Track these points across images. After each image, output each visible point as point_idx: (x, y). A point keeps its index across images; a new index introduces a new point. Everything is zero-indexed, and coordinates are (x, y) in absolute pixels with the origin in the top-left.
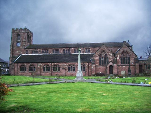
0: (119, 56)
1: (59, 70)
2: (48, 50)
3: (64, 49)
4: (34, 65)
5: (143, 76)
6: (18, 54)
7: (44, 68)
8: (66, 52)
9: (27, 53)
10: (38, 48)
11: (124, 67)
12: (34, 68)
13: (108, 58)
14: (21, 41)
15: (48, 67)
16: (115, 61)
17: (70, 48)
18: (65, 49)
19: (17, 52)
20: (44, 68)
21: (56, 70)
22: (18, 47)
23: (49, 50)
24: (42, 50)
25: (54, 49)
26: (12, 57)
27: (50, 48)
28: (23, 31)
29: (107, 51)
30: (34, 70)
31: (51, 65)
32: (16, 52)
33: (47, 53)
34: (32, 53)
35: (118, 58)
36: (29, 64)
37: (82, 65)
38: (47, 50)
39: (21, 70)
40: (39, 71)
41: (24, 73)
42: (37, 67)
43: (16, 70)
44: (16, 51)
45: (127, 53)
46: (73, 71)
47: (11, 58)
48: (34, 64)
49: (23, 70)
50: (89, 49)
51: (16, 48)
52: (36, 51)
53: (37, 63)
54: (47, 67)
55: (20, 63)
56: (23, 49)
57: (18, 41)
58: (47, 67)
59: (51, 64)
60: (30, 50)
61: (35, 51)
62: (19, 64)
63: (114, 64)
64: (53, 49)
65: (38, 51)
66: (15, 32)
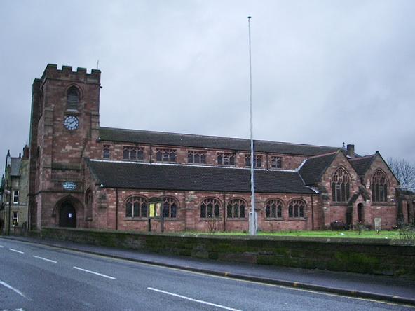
0: (369, 183)
1: (280, 215)
2: (175, 151)
3: (218, 153)
4: (172, 199)
5: (74, 242)
6: (70, 156)
7: (203, 207)
8: (165, 160)
9: (106, 156)
10: (144, 144)
11: (379, 208)
12: (142, 207)
14: (84, 114)
16: (362, 192)
17: (235, 151)
18: (222, 154)
19: (69, 148)
20: (202, 210)
21: (236, 215)
22: (71, 132)
23: (179, 150)
24: (157, 150)
25: (192, 152)
26: (52, 164)
27: (184, 147)
28: (89, 80)
29: (347, 167)
30: (173, 216)
31: (224, 199)
32: (63, 150)
33: (174, 160)
34: (126, 156)
36: (158, 192)
37: (168, 200)
38: (171, 150)
39: (128, 214)
40: (191, 216)
41: (140, 223)
42: (185, 205)
43: (114, 212)
44: (63, 145)
45: (381, 174)
46: (277, 219)
48: (172, 194)
49: (136, 215)
50: (205, 153)
51: (66, 136)
52: (137, 151)
53: (185, 190)
54: (210, 206)
55: (125, 188)
56: (94, 142)
57: (69, 110)
59: (224, 196)
61: (133, 152)
62: (124, 192)
63: (365, 201)
64: (189, 151)
65: (146, 152)
66: (60, 77)
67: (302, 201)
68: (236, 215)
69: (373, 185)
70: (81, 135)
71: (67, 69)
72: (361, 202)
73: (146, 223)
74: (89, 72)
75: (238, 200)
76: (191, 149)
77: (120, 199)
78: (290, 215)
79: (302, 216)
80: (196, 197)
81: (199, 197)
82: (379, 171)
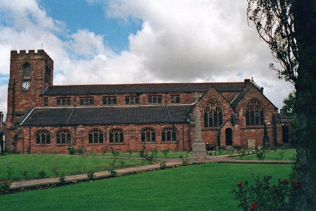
0: (242, 110)
1: (122, 140)
3: (126, 96)
7: (90, 136)
13: (221, 114)
15: (98, 133)
19: (24, 101)
21: (117, 141)
24: (80, 98)
35: (241, 113)
37: (149, 130)
44: (21, 100)
47: (11, 116)
56: (38, 97)
58: (96, 135)
60: (53, 99)
61: (155, 99)
63: (234, 126)
65: (72, 99)
67: (174, 129)
68: (117, 141)
69: (206, 115)
70: (31, 93)
71: (23, 52)
72: (229, 127)
73: (263, 130)
74: (36, 52)
75: (118, 130)
76: (104, 95)
77: (31, 132)
78: (163, 139)
79: (175, 139)
80: (84, 129)
81: (86, 129)
82: (254, 100)
